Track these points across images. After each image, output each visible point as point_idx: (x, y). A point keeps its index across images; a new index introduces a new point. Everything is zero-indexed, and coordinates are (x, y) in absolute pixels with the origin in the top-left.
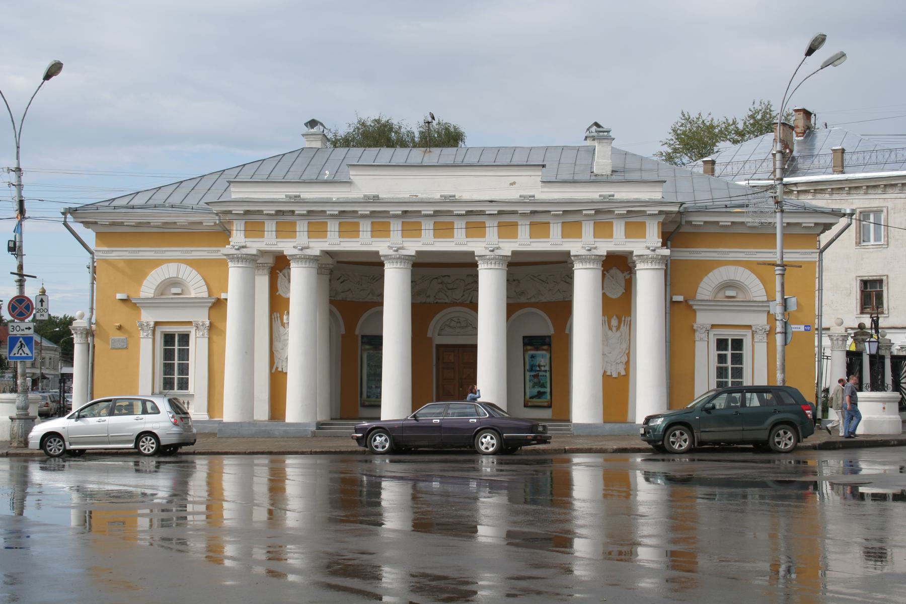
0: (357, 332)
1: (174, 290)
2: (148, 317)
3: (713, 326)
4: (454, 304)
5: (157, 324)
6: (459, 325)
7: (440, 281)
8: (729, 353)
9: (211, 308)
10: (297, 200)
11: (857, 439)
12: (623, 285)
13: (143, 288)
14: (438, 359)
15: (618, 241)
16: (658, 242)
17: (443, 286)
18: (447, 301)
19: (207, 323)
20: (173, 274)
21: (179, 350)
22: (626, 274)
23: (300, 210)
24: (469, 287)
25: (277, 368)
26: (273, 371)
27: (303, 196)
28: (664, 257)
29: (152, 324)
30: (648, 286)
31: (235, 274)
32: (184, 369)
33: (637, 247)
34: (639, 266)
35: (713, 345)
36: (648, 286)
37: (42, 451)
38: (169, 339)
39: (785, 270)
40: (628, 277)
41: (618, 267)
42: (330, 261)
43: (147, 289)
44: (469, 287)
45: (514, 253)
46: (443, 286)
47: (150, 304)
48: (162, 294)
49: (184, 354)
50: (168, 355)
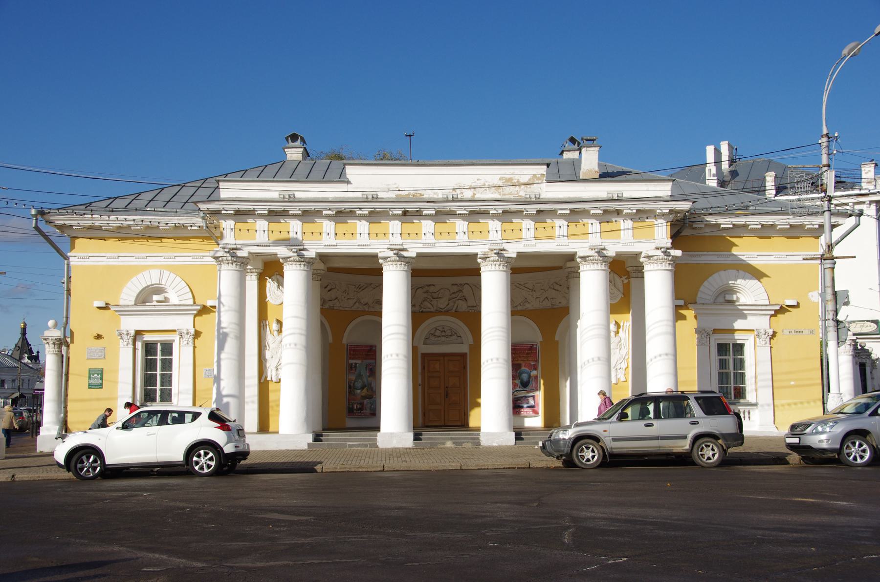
0: (344, 341)
1: (156, 298)
2: (131, 324)
3: (715, 331)
4: (439, 312)
5: (138, 333)
6: (443, 334)
7: (425, 290)
8: (731, 358)
9: (195, 316)
10: (292, 200)
11: (746, 448)
12: (622, 290)
13: (123, 296)
14: (423, 368)
15: (624, 239)
16: (668, 242)
17: (444, 288)
18: (432, 310)
19: (192, 331)
20: (155, 281)
21: (162, 360)
22: (624, 278)
23: (295, 209)
24: (454, 296)
25: (266, 377)
26: (262, 381)
27: (298, 195)
28: (675, 258)
29: (132, 333)
30: (657, 286)
31: (227, 275)
32: (167, 380)
33: (645, 248)
34: (647, 268)
35: (714, 350)
36: (657, 286)
37: (70, 475)
38: (150, 348)
39: (835, 263)
40: (626, 281)
41: (624, 273)
42: (321, 266)
43: (128, 296)
44: (454, 296)
45: (520, 255)
46: (444, 288)
47: (125, 311)
48: (144, 302)
49: (167, 365)
50: (150, 365)
